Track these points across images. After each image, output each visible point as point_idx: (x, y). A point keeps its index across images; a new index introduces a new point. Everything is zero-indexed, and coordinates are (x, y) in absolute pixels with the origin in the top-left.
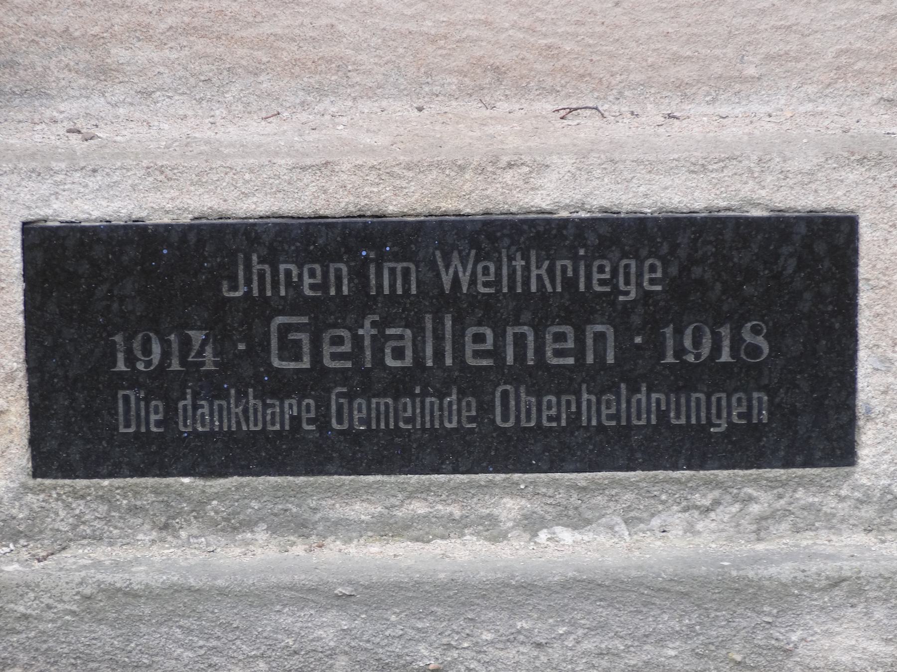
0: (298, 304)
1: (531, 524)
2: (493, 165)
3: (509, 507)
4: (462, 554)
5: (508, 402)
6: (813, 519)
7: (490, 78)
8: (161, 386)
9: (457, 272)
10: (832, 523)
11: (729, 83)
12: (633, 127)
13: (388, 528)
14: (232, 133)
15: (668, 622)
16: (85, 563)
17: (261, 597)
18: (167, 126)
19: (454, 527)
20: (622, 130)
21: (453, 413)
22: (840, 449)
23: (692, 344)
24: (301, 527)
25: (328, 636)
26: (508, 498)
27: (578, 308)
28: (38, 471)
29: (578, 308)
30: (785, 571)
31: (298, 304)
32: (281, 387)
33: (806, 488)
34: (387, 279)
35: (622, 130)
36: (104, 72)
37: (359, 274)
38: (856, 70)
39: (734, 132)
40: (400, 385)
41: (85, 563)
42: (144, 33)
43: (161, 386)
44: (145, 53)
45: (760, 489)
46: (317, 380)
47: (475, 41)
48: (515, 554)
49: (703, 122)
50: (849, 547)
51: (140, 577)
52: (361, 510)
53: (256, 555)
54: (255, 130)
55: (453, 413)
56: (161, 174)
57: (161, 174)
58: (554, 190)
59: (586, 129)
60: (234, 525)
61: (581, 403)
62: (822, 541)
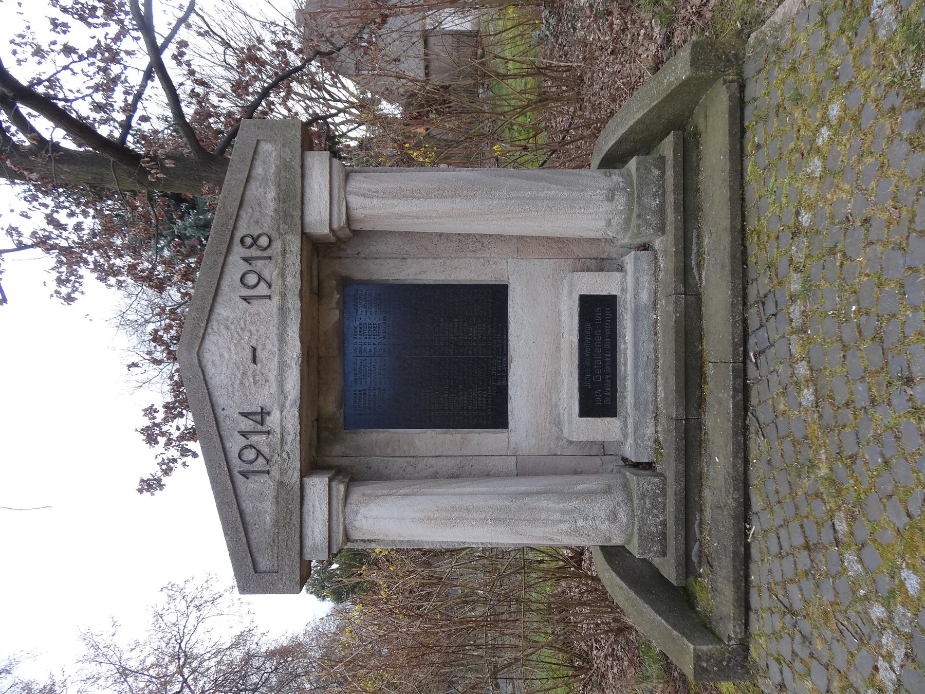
0: (591, 377)
1: (625, 343)
2: (571, 348)
3: (622, 346)
4: (629, 353)
5: (731, 501)
6: (625, 301)
7: (558, 349)
8: (603, 397)
9: (587, 353)
10: (625, 299)
11: (559, 313)
12: (566, 328)
13: (625, 365)
14: (566, 387)
15: (640, 323)
16: (630, 409)
17: (636, 383)
18: (564, 396)
19: (625, 354)
20: (566, 329)
21: (608, 354)
22: (615, 297)
23: (598, 319)
24: (625, 377)
25: (642, 373)
26: (621, 346)
27: (593, 336)
28: (616, 416)
29: (593, 336)
30: (633, 305)
31: (591, 377)
32: (604, 380)
33: (620, 302)
34: (588, 364)
35: (566, 329)
36: (556, 405)
37: (587, 368)
38: (105, 112)
39: (567, 313)
40: (604, 362)
41: (630, 409)
42: (551, 399)
43: (603, 397)
44: (553, 399)
45: (620, 309)
46: (603, 374)
47: (658, 65)
48: (630, 346)
49: (565, 318)
50: (629, 296)
51: (633, 401)
52: (623, 369)
53: (629, 384)
54: (565, 383)
55: (608, 354)
56: (572, 397)
57: (572, 397)
58: (576, 340)
59: (566, 334)
60: (625, 387)
61: (665, 389)
62: (628, 300)
